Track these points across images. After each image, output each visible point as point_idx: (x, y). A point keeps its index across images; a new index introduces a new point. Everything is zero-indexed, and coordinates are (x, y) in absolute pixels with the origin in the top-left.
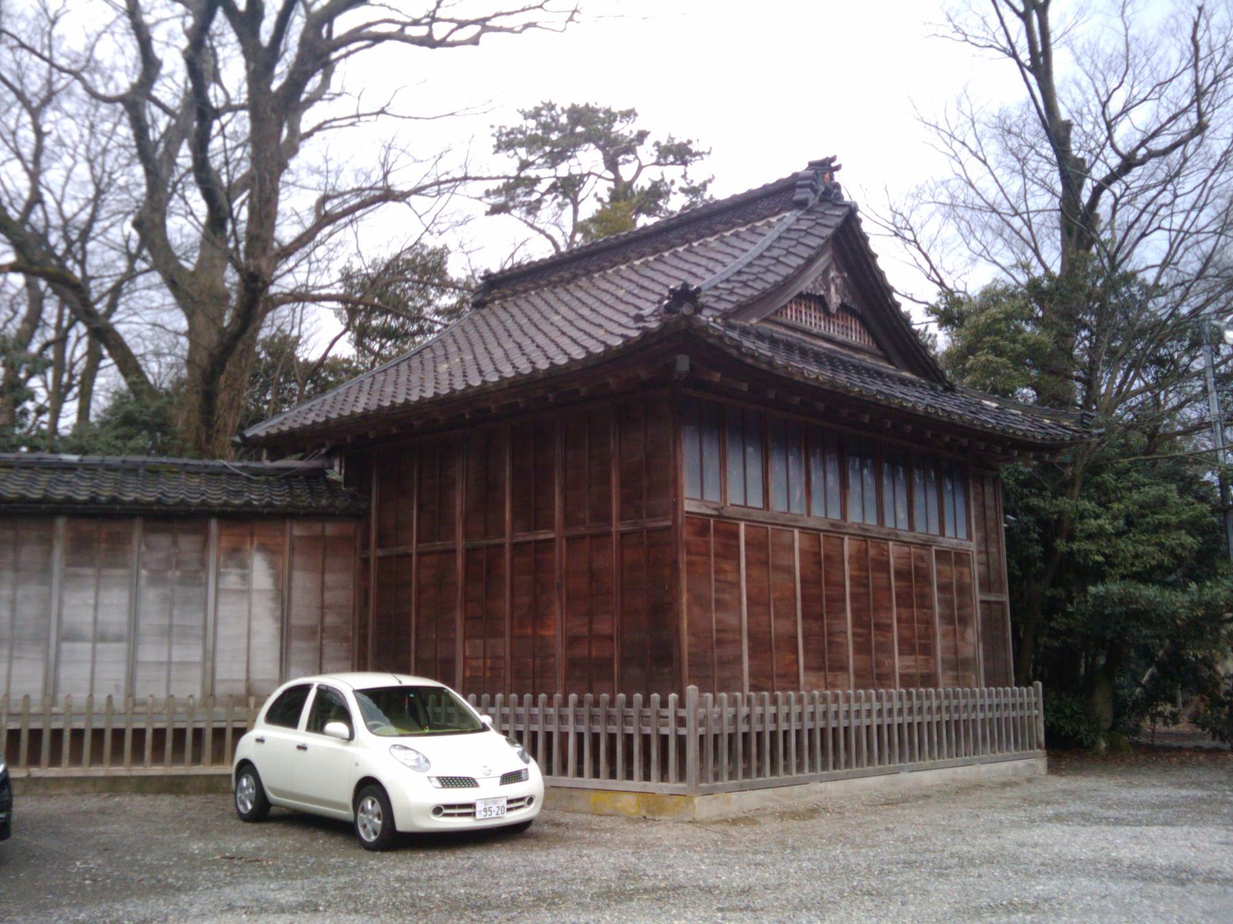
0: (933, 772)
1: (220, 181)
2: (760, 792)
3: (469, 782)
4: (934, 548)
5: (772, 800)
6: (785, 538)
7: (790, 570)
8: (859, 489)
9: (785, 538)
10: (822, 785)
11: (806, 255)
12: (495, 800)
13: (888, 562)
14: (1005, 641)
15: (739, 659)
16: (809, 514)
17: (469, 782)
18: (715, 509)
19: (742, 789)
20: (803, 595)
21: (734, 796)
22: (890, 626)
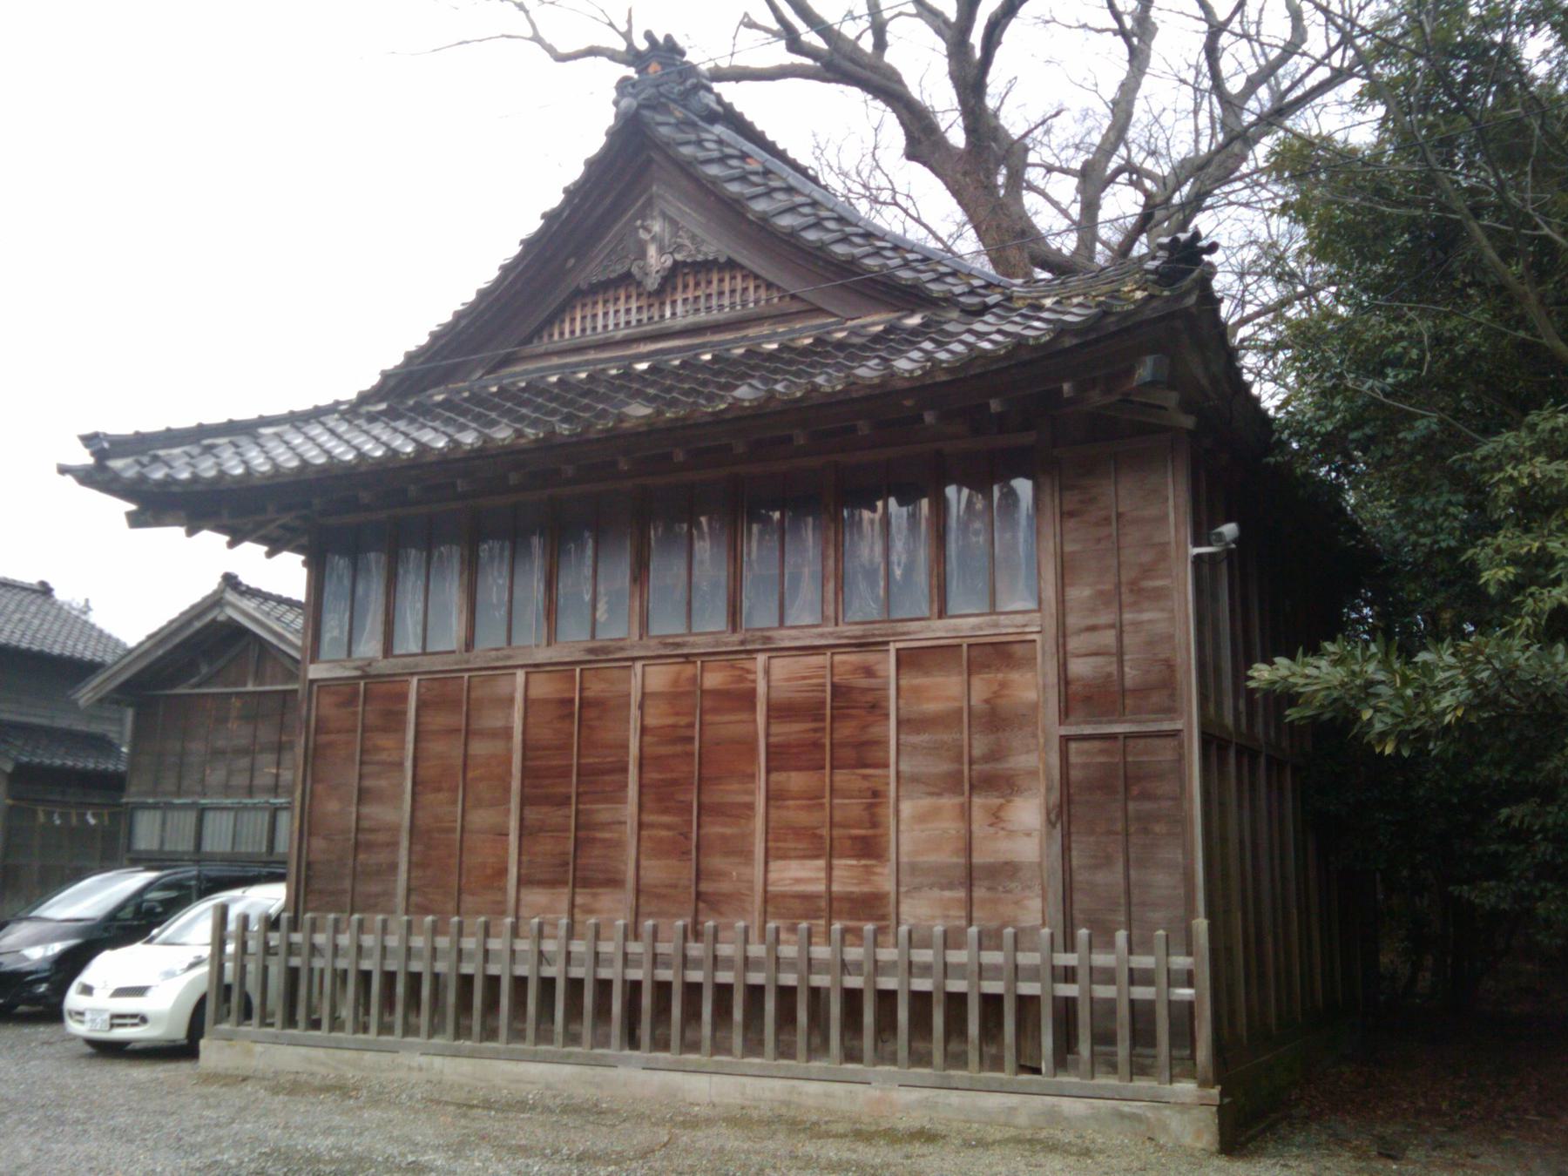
0: (716, 1078)
1: (985, 351)
2: (303, 1050)
3: (139, 991)
4: (892, 647)
5: (323, 1064)
6: (502, 687)
7: (507, 733)
8: (420, 606)
9: (502, 687)
10: (424, 1060)
11: (1077, 165)
12: (100, 1011)
13: (753, 692)
14: (1183, 822)
15: (393, 867)
16: (781, 625)
17: (139, 991)
18: (356, 668)
19: (276, 1040)
20: (524, 769)
21: (259, 1048)
22: (750, 806)
